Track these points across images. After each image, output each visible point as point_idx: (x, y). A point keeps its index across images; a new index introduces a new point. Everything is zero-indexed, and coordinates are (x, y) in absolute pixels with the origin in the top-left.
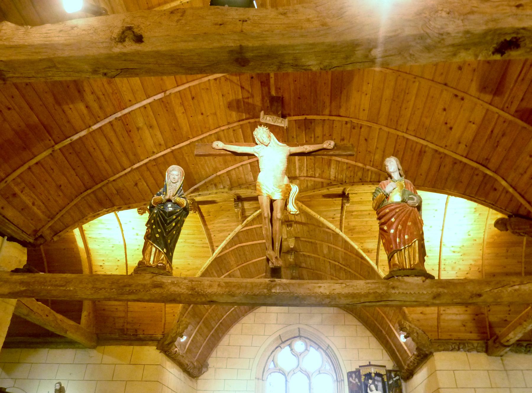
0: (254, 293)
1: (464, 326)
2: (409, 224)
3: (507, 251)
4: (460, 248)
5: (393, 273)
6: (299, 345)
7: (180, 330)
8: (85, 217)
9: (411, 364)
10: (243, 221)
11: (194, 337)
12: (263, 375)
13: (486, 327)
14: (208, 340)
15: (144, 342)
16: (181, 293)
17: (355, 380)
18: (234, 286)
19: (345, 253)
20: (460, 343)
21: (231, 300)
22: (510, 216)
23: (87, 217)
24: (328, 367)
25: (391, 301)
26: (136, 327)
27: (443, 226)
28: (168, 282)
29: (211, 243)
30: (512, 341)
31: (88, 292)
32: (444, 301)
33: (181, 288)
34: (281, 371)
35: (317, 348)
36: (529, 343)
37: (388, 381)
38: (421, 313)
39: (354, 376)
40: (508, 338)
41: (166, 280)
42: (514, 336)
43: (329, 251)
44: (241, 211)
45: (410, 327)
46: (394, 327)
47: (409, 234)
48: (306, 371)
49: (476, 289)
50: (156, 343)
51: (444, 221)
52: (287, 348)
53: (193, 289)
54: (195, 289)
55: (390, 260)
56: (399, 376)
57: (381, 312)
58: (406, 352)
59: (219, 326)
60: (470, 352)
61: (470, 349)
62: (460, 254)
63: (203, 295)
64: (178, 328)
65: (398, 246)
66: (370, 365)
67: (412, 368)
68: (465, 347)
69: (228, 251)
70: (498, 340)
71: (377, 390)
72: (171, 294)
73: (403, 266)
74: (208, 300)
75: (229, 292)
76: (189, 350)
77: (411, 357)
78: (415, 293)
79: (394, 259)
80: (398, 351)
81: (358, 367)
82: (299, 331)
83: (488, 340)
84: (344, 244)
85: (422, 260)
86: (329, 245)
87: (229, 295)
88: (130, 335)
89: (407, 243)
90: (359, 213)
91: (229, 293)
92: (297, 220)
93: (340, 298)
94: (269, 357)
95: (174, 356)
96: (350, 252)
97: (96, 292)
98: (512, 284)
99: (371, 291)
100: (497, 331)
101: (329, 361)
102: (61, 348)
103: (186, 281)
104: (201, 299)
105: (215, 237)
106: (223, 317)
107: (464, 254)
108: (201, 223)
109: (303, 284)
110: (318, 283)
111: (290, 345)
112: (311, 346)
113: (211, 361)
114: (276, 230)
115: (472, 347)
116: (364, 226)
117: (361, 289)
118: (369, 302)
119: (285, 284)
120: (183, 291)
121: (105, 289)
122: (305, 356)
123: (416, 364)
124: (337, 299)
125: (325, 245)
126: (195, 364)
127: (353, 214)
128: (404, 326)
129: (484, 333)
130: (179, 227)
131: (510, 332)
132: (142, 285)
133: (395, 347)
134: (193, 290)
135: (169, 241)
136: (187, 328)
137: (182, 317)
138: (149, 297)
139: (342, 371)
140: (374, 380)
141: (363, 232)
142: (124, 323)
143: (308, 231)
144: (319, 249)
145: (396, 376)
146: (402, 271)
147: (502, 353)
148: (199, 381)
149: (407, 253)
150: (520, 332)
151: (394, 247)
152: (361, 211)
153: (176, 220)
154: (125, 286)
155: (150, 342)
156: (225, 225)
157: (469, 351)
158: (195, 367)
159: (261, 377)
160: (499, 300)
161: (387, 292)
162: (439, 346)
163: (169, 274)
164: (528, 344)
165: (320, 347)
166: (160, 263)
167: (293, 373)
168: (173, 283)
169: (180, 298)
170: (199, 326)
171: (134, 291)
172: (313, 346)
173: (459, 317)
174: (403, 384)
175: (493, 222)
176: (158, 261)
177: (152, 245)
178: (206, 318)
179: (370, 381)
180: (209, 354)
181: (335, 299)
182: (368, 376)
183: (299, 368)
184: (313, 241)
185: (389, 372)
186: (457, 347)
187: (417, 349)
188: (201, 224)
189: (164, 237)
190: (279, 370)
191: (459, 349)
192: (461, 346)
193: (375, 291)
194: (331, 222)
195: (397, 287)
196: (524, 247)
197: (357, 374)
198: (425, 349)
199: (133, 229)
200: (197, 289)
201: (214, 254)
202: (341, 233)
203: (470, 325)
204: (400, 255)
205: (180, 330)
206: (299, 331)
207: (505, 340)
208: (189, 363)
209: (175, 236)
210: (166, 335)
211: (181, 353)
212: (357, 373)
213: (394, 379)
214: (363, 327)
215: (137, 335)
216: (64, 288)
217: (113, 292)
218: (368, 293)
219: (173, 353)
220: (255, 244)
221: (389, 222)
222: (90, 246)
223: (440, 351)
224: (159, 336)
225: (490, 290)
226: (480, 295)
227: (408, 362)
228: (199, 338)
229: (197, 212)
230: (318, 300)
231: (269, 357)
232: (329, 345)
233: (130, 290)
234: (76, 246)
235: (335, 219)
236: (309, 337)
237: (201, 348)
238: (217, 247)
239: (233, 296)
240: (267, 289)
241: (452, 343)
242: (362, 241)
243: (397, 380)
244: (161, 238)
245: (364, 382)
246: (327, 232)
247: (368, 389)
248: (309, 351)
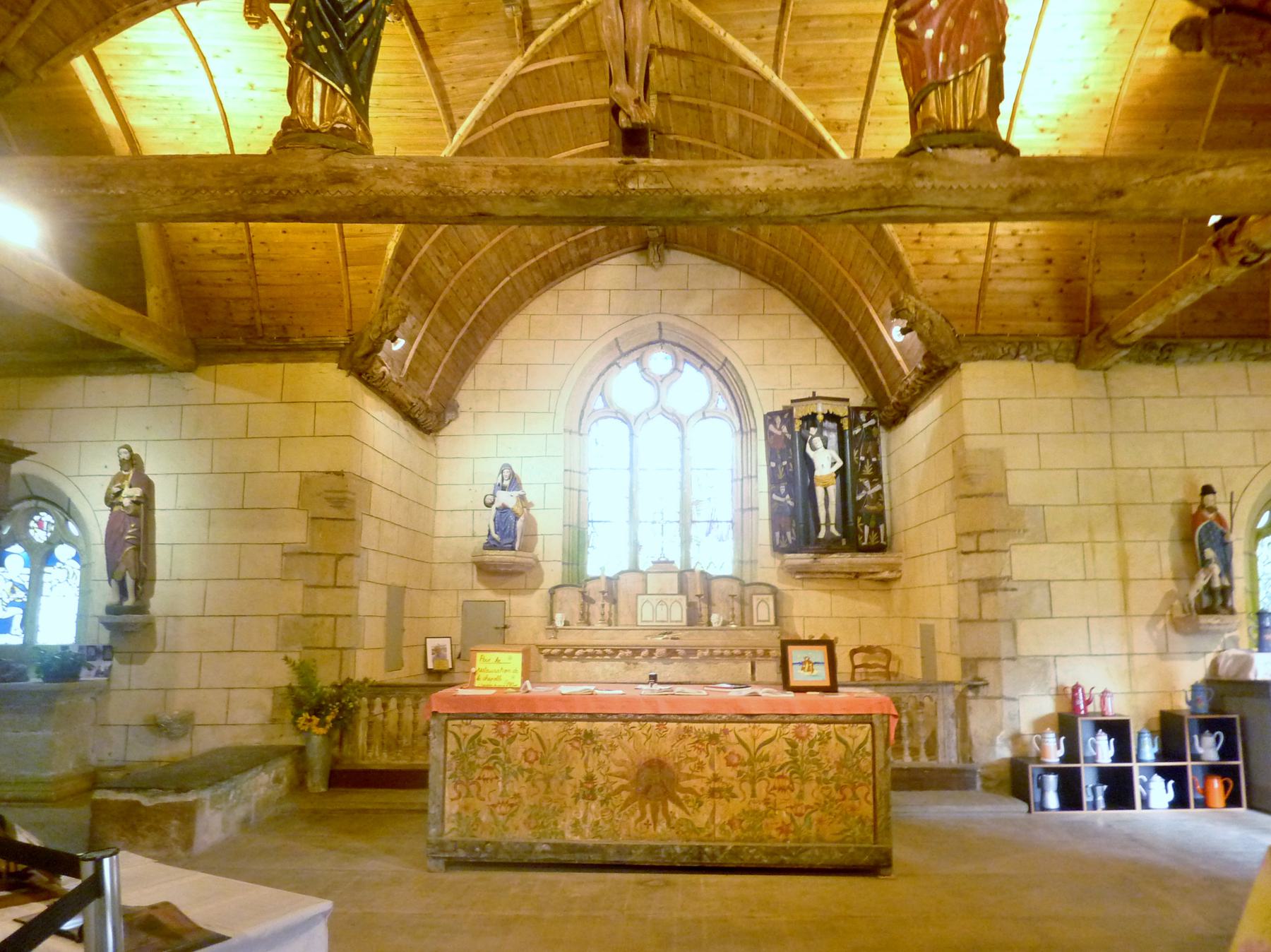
0: (584, 191)
1: (1036, 305)
2: (974, 14)
3: (1167, 131)
4: (1058, 120)
5: (922, 140)
6: (660, 360)
7: (390, 324)
8: (111, 15)
9: (907, 391)
10: (527, 46)
11: (421, 345)
12: (580, 424)
13: (1083, 309)
14: (454, 351)
15: (311, 354)
16: (402, 194)
17: (780, 429)
18: (534, 176)
19: (780, 133)
20: (1021, 343)
21: (527, 209)
22: (1214, 12)
23: (118, 16)
24: (723, 403)
25: (912, 206)
26: (284, 319)
27: (1027, 62)
28: (366, 169)
29: (446, 107)
30: (1138, 335)
31: (167, 200)
32: (1034, 206)
33: (400, 182)
34: (619, 415)
35: (699, 366)
36: (1167, 341)
37: (851, 431)
38: (946, 277)
39: (778, 420)
40: (1129, 329)
41: (358, 163)
42: (1143, 325)
43: (742, 131)
44: (520, 14)
45: (916, 308)
46: (877, 312)
47: (972, 42)
48: (673, 414)
49: (1112, 179)
50: (335, 355)
51: (1031, 48)
52: (633, 368)
53: (431, 184)
54: (436, 184)
55: (914, 110)
56: (876, 418)
57: (851, 280)
58: (899, 365)
59: (475, 320)
60: (1041, 361)
61: (1041, 356)
62: (1055, 136)
63: (458, 199)
64: (384, 318)
65: (940, 72)
66: (814, 398)
67: (907, 399)
68: (1032, 351)
69: (489, 129)
70: (1106, 334)
71: (826, 447)
72: (379, 199)
73: (948, 124)
74: (472, 210)
75: (522, 190)
76: (413, 372)
77: (909, 376)
78: (969, 187)
79: (926, 109)
80: (880, 366)
81: (789, 404)
82: (660, 329)
83: (1084, 335)
84: (780, 111)
85: (994, 112)
86: (745, 113)
87: (522, 197)
88: (271, 339)
89: (962, 65)
90: (826, 23)
91: (523, 194)
92: (664, 43)
93: (791, 201)
94: (593, 386)
95: (378, 384)
96: (794, 130)
97: (187, 198)
98: (1198, 167)
99: (867, 184)
100: (1106, 316)
101: (726, 391)
102: (110, 374)
103: (412, 166)
104: (453, 209)
105: (455, 92)
106: (484, 298)
107: (1065, 137)
108: (417, 52)
109: (703, 169)
110: (740, 166)
111: (639, 361)
112: (685, 361)
113: (463, 398)
114: (635, 29)
115: (1046, 350)
116: (835, 58)
117: (844, 179)
118: (860, 210)
119: (660, 170)
120: (407, 190)
121: (207, 189)
122: (672, 382)
123: (918, 392)
124: (785, 204)
125: (732, 113)
126: (429, 403)
127: (810, 25)
128: (905, 306)
129: (1078, 321)
130: (374, 29)
131: (1138, 316)
132: (300, 177)
133: (875, 357)
134: (431, 186)
135: (355, 64)
136: (404, 318)
137: (391, 295)
138: (324, 208)
139: (753, 412)
140: (821, 429)
141: (830, 77)
142: (254, 311)
143: (693, 77)
144: (715, 125)
145: (868, 418)
146: (944, 135)
147: (1110, 362)
148: (440, 440)
149: (960, 90)
150: (1161, 314)
151: (930, 76)
152: (831, 17)
153: (364, 8)
154: (258, 181)
155: (321, 354)
156: (481, 57)
157: (1037, 359)
158: (428, 411)
159: (575, 429)
160: (1161, 206)
161: (905, 186)
162: (975, 348)
163: (365, 149)
164: (1168, 345)
165: (706, 363)
166: (338, 122)
167: (646, 417)
168: (378, 171)
169: (401, 206)
170: (428, 320)
171: (284, 192)
172: (692, 361)
173: (1028, 286)
174: (883, 435)
175: (1174, 21)
176: (334, 118)
177: (311, 74)
178: (446, 302)
179: (813, 431)
180: (459, 382)
181: (780, 203)
182: (810, 419)
183: (659, 409)
184: (702, 102)
185: (857, 410)
186: (1013, 352)
187: (925, 357)
188: (417, 55)
189: (340, 53)
190: (617, 412)
191: (1017, 356)
192: (1023, 350)
193: (875, 183)
194: (753, 48)
195: (930, 175)
196: (1208, 120)
197: (786, 416)
198: (942, 357)
199: (239, 71)
200: (441, 185)
201: (456, 138)
202: (776, 80)
203: (1050, 303)
204: (943, 98)
205: (389, 324)
206: (660, 329)
207: (1123, 331)
208: (415, 401)
209: (368, 53)
210: (356, 338)
211: (395, 376)
212: (786, 413)
213: (865, 426)
214: (807, 318)
215: (287, 339)
216: (102, 191)
217: (231, 197)
218: (860, 187)
219: (376, 377)
220: (558, 112)
221: (924, 11)
222: (134, 121)
223: (975, 359)
224: (342, 339)
225: (1146, 182)
226: (1119, 193)
227: (901, 388)
228: (433, 346)
229: (403, 20)
230: (739, 205)
231: (593, 386)
232: (726, 359)
233: (271, 191)
234: (97, 122)
235: (764, 39)
236: (682, 343)
237: (440, 370)
238: (462, 118)
239: (533, 199)
240: (615, 181)
241: (1004, 342)
242: (826, 101)
243: (871, 427)
244: (334, 56)
245: (800, 432)
246: (741, 77)
247: (808, 445)
248: (681, 372)
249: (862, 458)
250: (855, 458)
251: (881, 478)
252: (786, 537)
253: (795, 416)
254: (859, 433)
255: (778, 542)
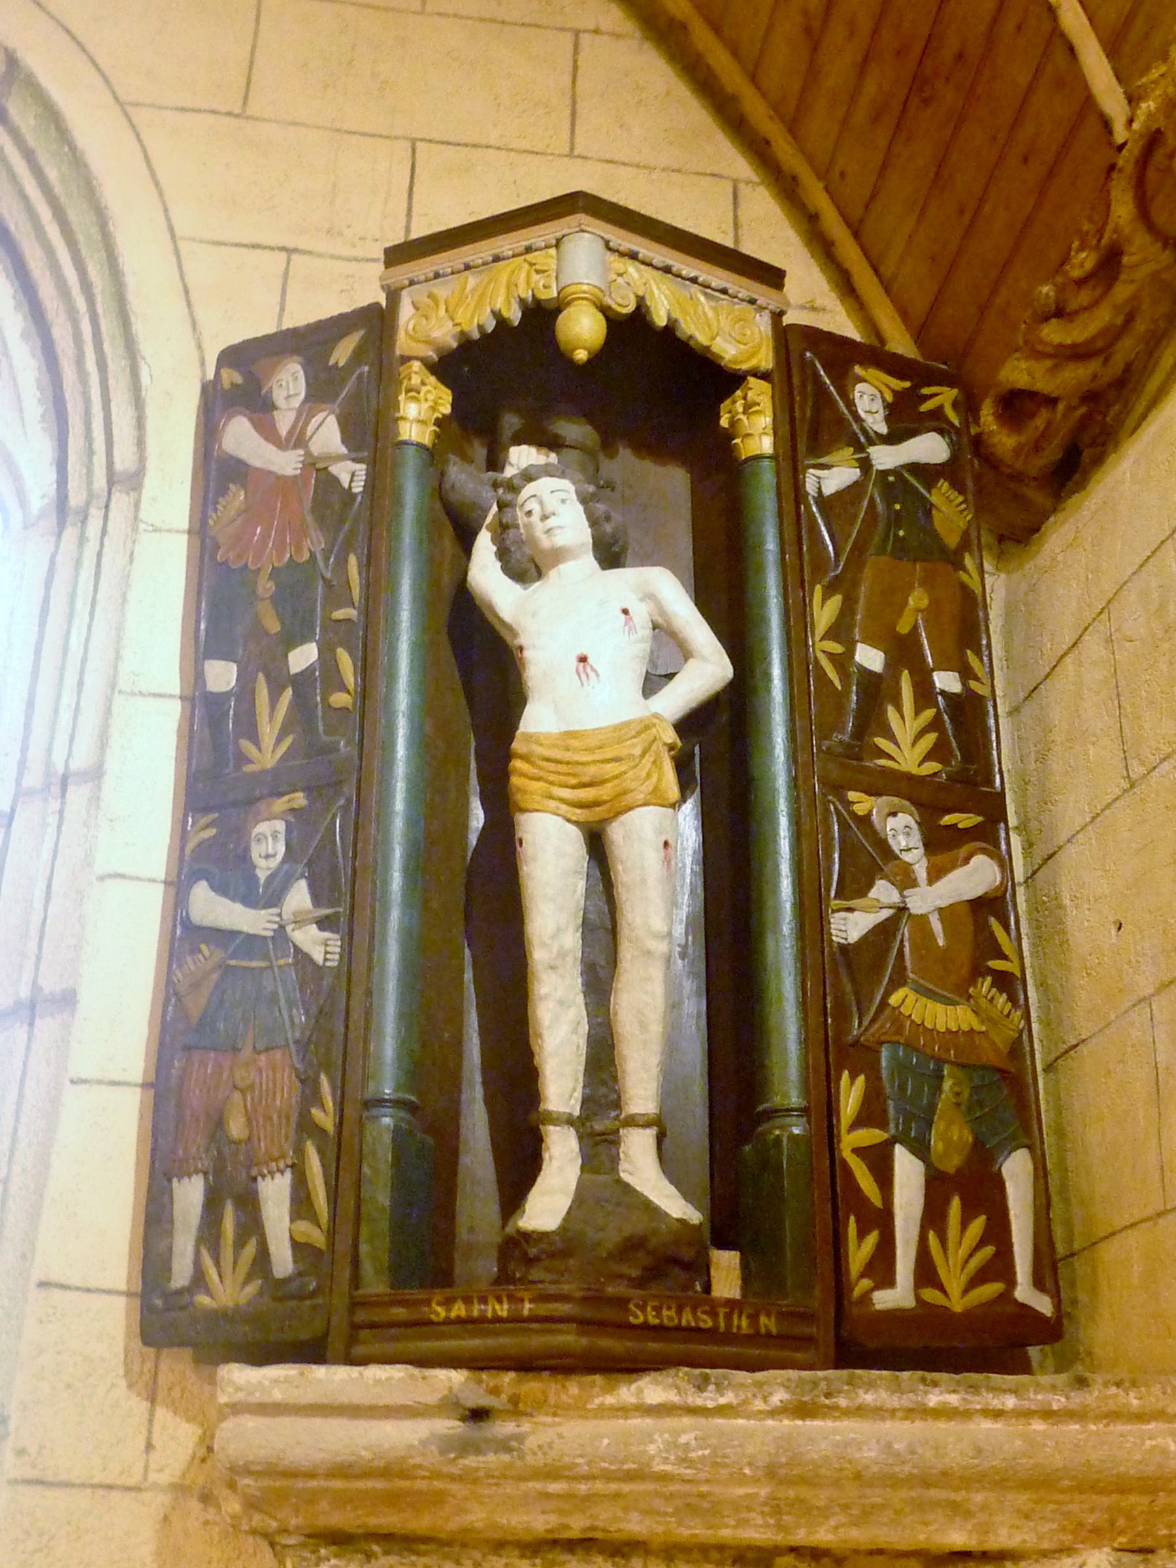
197: (342, 354)
245: (433, 456)
247: (484, 545)
249: (870, 658)
250: (822, 648)
251: (994, 809)
252: (249, 1204)
253: (403, 343)
254: (852, 492)
255: (181, 1274)
